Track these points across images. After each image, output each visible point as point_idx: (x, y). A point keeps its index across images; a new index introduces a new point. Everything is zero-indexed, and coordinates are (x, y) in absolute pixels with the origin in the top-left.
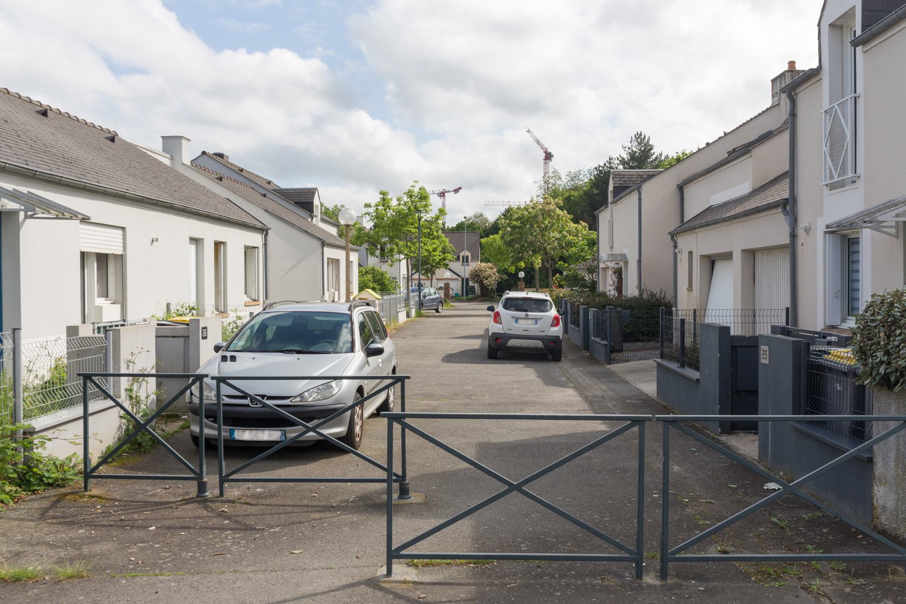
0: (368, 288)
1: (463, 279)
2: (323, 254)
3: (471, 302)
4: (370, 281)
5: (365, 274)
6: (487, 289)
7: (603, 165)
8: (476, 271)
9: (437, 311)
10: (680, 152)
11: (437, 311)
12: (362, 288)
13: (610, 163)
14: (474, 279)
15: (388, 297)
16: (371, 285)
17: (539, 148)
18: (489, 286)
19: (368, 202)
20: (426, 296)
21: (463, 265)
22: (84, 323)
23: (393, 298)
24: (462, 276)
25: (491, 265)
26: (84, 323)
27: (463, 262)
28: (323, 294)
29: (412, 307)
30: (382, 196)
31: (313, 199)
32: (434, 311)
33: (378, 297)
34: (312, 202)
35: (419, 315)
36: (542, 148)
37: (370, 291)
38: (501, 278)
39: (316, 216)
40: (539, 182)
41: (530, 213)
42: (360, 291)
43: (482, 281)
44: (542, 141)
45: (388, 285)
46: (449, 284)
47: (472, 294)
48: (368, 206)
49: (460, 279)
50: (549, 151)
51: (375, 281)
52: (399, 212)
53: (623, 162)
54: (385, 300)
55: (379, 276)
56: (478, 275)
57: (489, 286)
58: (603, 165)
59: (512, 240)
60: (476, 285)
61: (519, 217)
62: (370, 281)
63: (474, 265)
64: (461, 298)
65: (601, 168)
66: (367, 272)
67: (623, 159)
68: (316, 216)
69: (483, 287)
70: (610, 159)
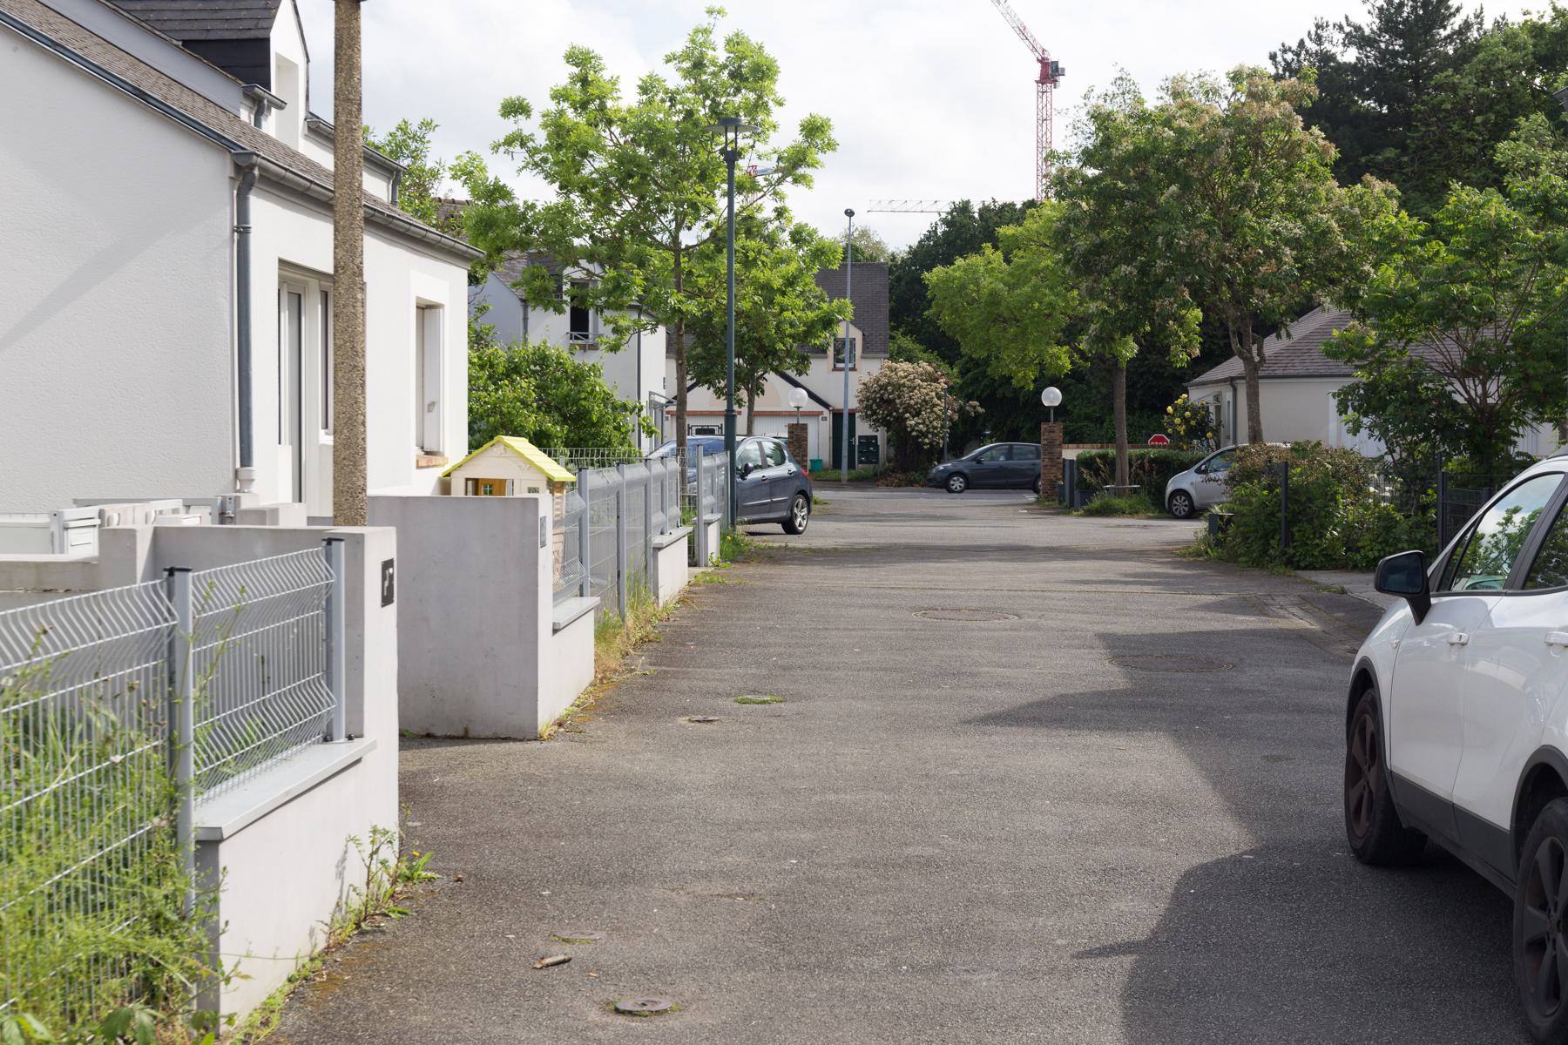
0: (516, 432)
1: (837, 416)
2: (242, 230)
3: (862, 489)
4: (525, 404)
5: (507, 375)
6: (919, 446)
7: (1294, 47)
8: (883, 387)
9: (790, 527)
10: (1534, 11)
11: (790, 527)
12: (483, 431)
13: (1319, 40)
14: (875, 413)
15: (610, 476)
16: (531, 421)
17: (1024, 47)
18: (925, 435)
19: (513, 94)
20: (747, 470)
21: (835, 369)
22: (300, 501)
23: (631, 484)
24: (838, 404)
25: (930, 369)
26: (300, 501)
27: (837, 360)
28: (246, 459)
29: (707, 517)
30: (576, 70)
31: (269, 28)
32: (778, 528)
33: (560, 473)
34: (265, 43)
35: (734, 553)
36: (1034, 49)
37: (522, 444)
38: (961, 411)
39: (280, 105)
40: (1072, 112)
41: (1180, 132)
42: (474, 446)
43: (901, 420)
44: (1032, 30)
45: (600, 423)
46: (804, 428)
47: (868, 462)
48: (515, 108)
49: (826, 413)
50: (1052, 58)
51: (546, 408)
52: (648, 133)
53: (1357, 38)
54: (595, 493)
55: (566, 387)
56: (890, 402)
57: (925, 435)
58: (1294, 47)
59: (1099, 249)
60: (881, 435)
61: (1137, 149)
62: (525, 404)
63: (870, 369)
64: (833, 474)
65: (1289, 56)
66: (513, 370)
67: (1358, 29)
68: (280, 105)
69: (904, 441)
70: (1318, 26)
